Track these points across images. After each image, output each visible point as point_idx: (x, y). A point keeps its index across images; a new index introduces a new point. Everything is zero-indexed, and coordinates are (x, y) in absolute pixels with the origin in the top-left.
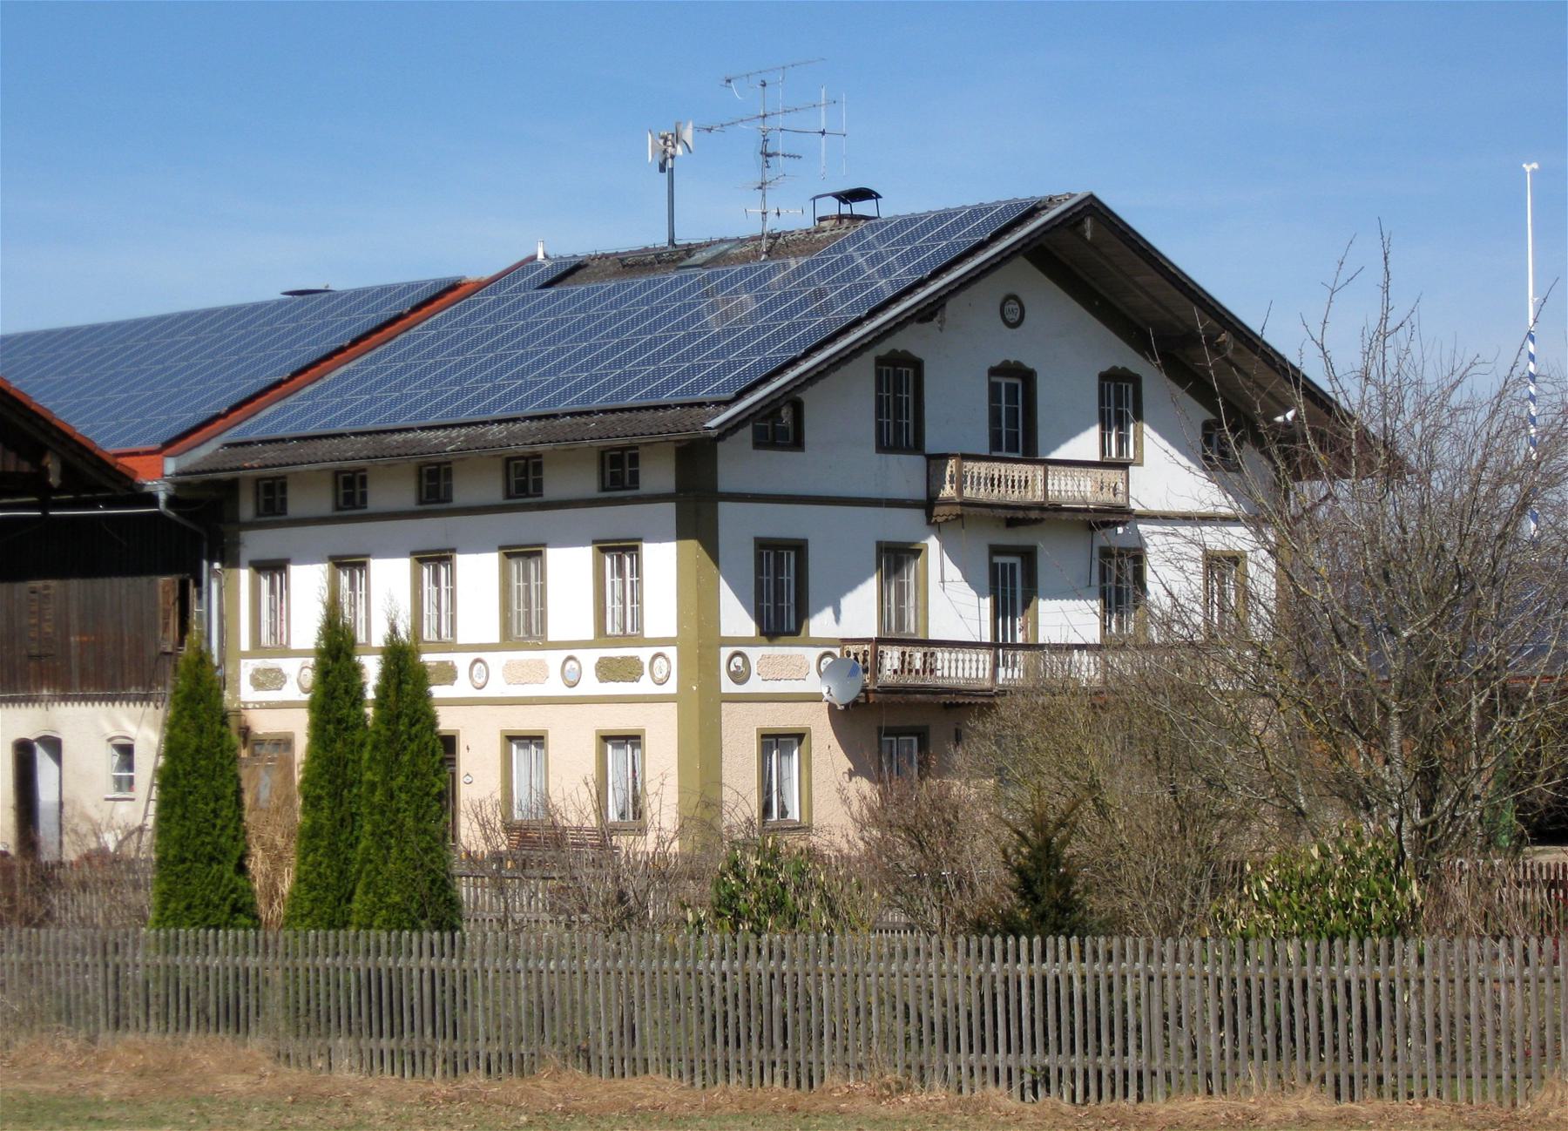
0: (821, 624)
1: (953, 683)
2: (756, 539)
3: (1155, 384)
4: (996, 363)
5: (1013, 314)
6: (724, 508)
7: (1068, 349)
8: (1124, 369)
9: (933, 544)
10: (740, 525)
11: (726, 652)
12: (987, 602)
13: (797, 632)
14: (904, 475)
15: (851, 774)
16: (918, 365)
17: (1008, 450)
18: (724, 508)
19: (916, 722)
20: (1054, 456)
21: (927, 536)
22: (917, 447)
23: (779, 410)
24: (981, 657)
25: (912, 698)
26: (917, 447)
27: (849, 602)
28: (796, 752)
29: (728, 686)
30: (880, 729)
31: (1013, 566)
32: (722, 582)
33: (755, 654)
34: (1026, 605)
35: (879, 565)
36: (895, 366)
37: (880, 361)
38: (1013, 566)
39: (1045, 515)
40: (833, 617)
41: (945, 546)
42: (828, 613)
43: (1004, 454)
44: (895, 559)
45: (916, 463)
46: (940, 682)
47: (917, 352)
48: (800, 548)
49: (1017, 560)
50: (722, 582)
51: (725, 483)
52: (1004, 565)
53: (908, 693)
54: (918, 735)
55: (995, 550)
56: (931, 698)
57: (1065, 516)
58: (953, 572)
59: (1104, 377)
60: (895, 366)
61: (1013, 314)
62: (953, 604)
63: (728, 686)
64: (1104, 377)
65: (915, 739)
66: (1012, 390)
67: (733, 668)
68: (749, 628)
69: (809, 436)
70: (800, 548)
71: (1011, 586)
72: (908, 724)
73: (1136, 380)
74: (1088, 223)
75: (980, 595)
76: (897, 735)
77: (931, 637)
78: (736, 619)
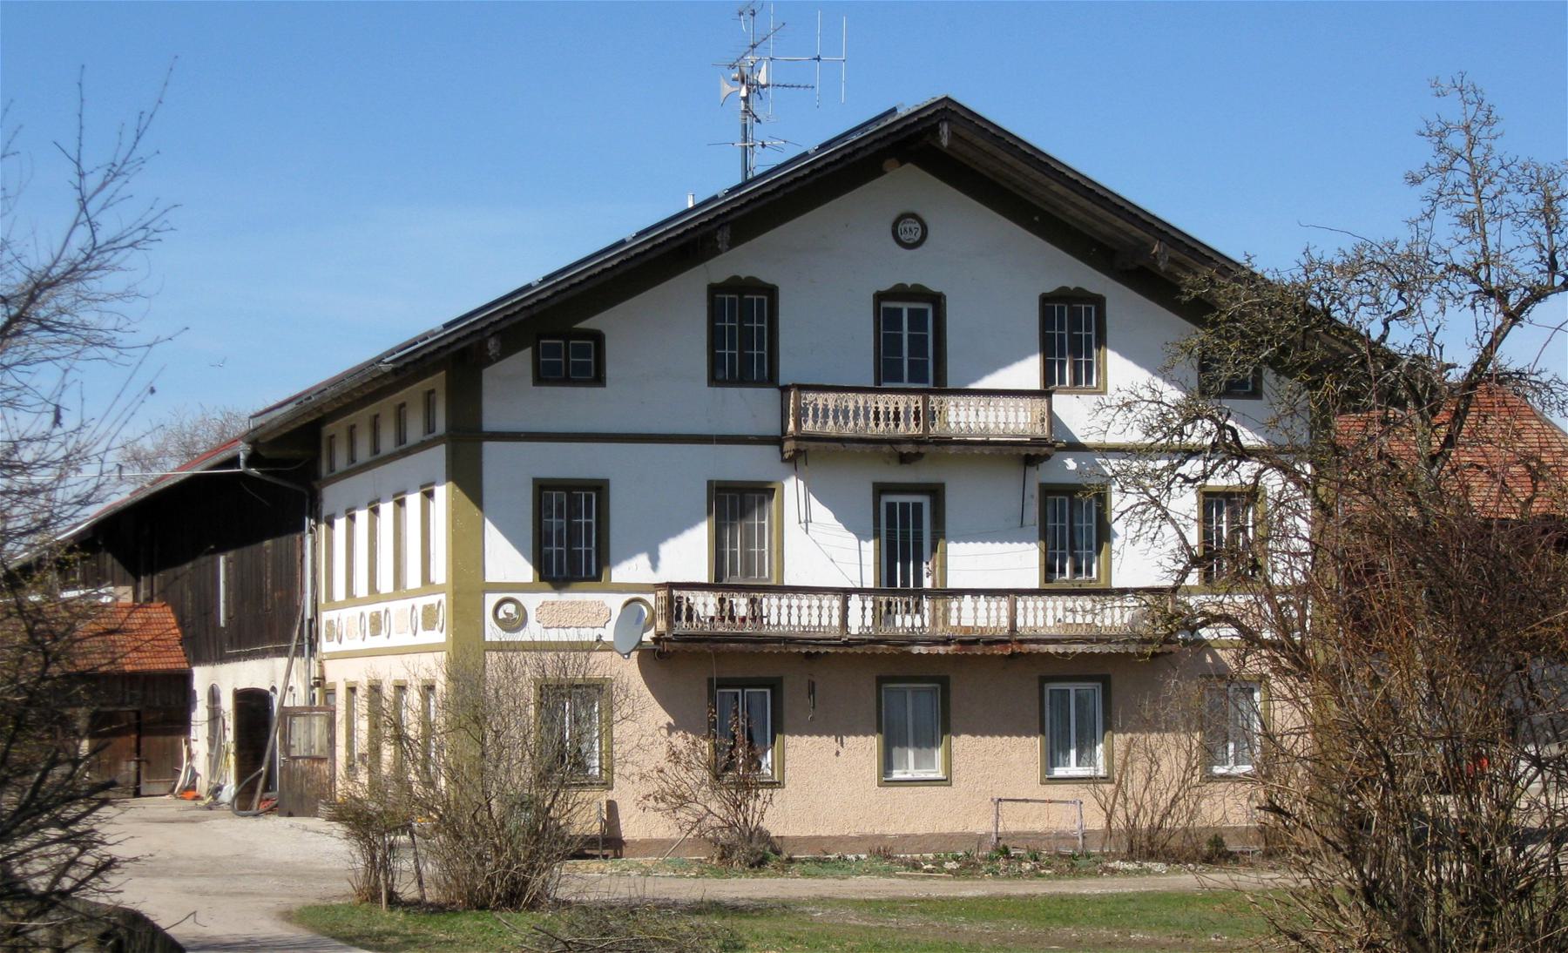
0: (630, 570)
1: (784, 631)
2: (535, 480)
3: (1122, 304)
4: (886, 286)
5: (909, 232)
6: (489, 447)
7: (989, 271)
8: (1078, 289)
9: (792, 489)
10: (510, 469)
11: (491, 600)
12: (869, 547)
13: (598, 578)
14: (750, 408)
15: (670, 729)
16: (772, 292)
17: (911, 380)
18: (489, 447)
19: (767, 672)
20: (973, 386)
21: (787, 477)
22: (771, 379)
23: (485, 341)
24: (825, 603)
25: (767, 649)
26: (771, 379)
27: (668, 549)
28: (1100, 748)
29: (493, 633)
30: (710, 680)
31: (918, 507)
32: (487, 522)
33: (531, 601)
34: (934, 549)
35: (709, 513)
36: (741, 295)
37: (713, 290)
38: (918, 507)
39: (923, 449)
40: (648, 563)
41: (811, 488)
42: (642, 560)
43: (906, 385)
44: (735, 505)
45: (771, 394)
46: (765, 631)
47: (766, 277)
48: (600, 488)
49: (925, 501)
50: (487, 522)
51: (490, 422)
52: (904, 506)
53: (718, 641)
54: (772, 687)
55: (880, 489)
56: (751, 647)
57: (952, 450)
58: (822, 514)
59: (1045, 299)
60: (741, 295)
61: (909, 232)
62: (821, 552)
63: (493, 633)
64: (1045, 299)
65: (768, 691)
66: (917, 319)
67: (501, 615)
68: (525, 572)
69: (611, 371)
70: (600, 488)
71: (906, 534)
72: (739, 675)
73: (1099, 301)
74: (945, 128)
75: (861, 536)
76: (743, 687)
77: (786, 583)
78: (506, 561)
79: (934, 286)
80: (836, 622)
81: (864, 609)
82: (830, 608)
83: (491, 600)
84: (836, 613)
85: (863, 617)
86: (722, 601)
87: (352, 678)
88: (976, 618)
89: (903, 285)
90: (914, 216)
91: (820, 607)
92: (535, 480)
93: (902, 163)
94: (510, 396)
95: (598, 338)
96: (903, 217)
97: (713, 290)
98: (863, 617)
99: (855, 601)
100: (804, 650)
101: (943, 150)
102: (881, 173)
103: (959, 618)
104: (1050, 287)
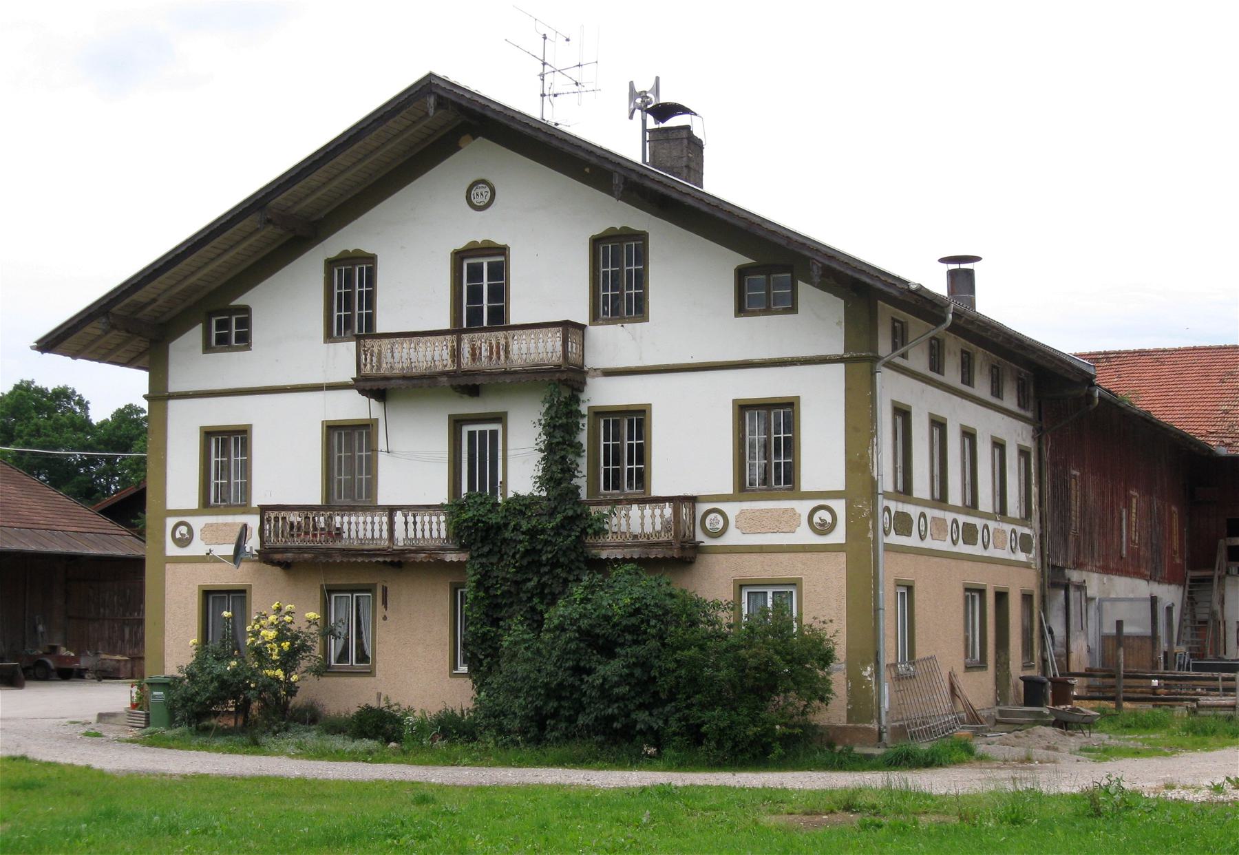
2: (251, 426)
4: (460, 245)
16: (372, 259)
33: (198, 523)
47: (369, 249)
52: (483, 433)
55: (457, 423)
59: (596, 242)
79: (500, 241)
80: (385, 534)
81: (406, 523)
82: (381, 524)
83: (171, 522)
84: (385, 527)
85: (407, 530)
86: (307, 518)
87: (1002, 585)
88: (642, 525)
89: (347, 251)
90: (483, 182)
91: (373, 523)
92: (251, 426)
93: (474, 138)
94: (817, 324)
95: (246, 310)
96: (475, 184)
97: (330, 264)
98: (407, 530)
99: (399, 517)
100: (374, 560)
101: (434, 128)
102: (458, 148)
103: (628, 524)
104: (598, 230)
